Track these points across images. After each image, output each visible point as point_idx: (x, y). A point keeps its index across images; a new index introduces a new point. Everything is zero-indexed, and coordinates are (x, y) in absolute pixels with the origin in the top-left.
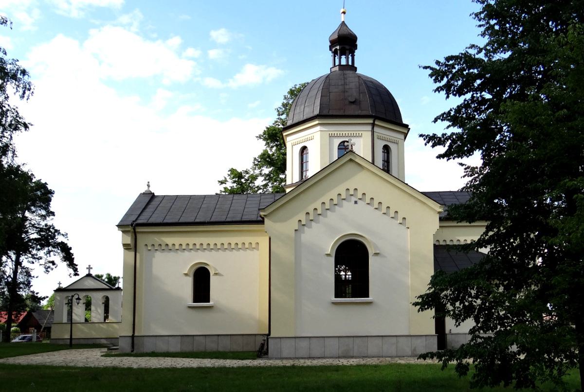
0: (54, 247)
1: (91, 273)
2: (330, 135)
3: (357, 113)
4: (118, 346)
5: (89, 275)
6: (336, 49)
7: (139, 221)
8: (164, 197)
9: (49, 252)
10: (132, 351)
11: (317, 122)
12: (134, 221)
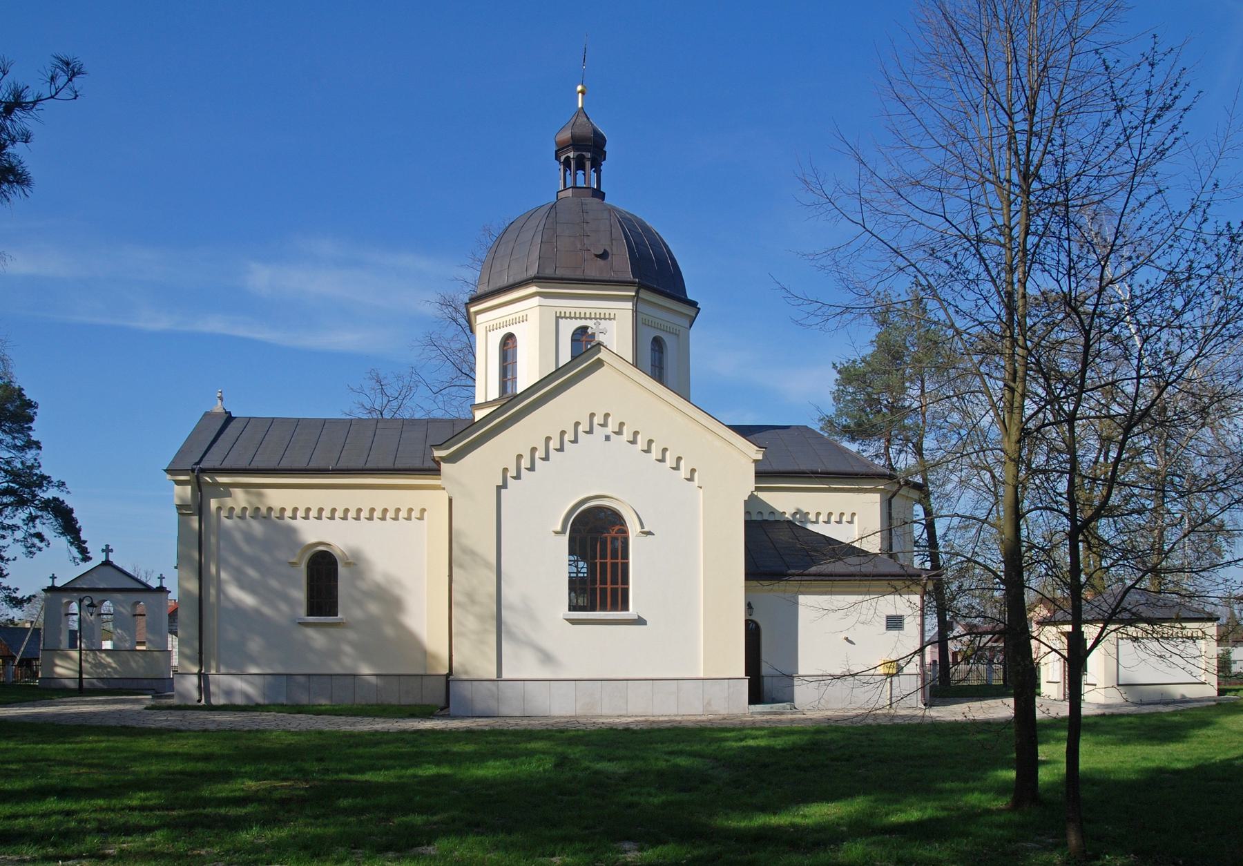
0: (41, 509)
2: (558, 315)
3: (605, 277)
4: (170, 696)
5: (107, 563)
6: (568, 159)
9: (32, 519)
11: (533, 289)
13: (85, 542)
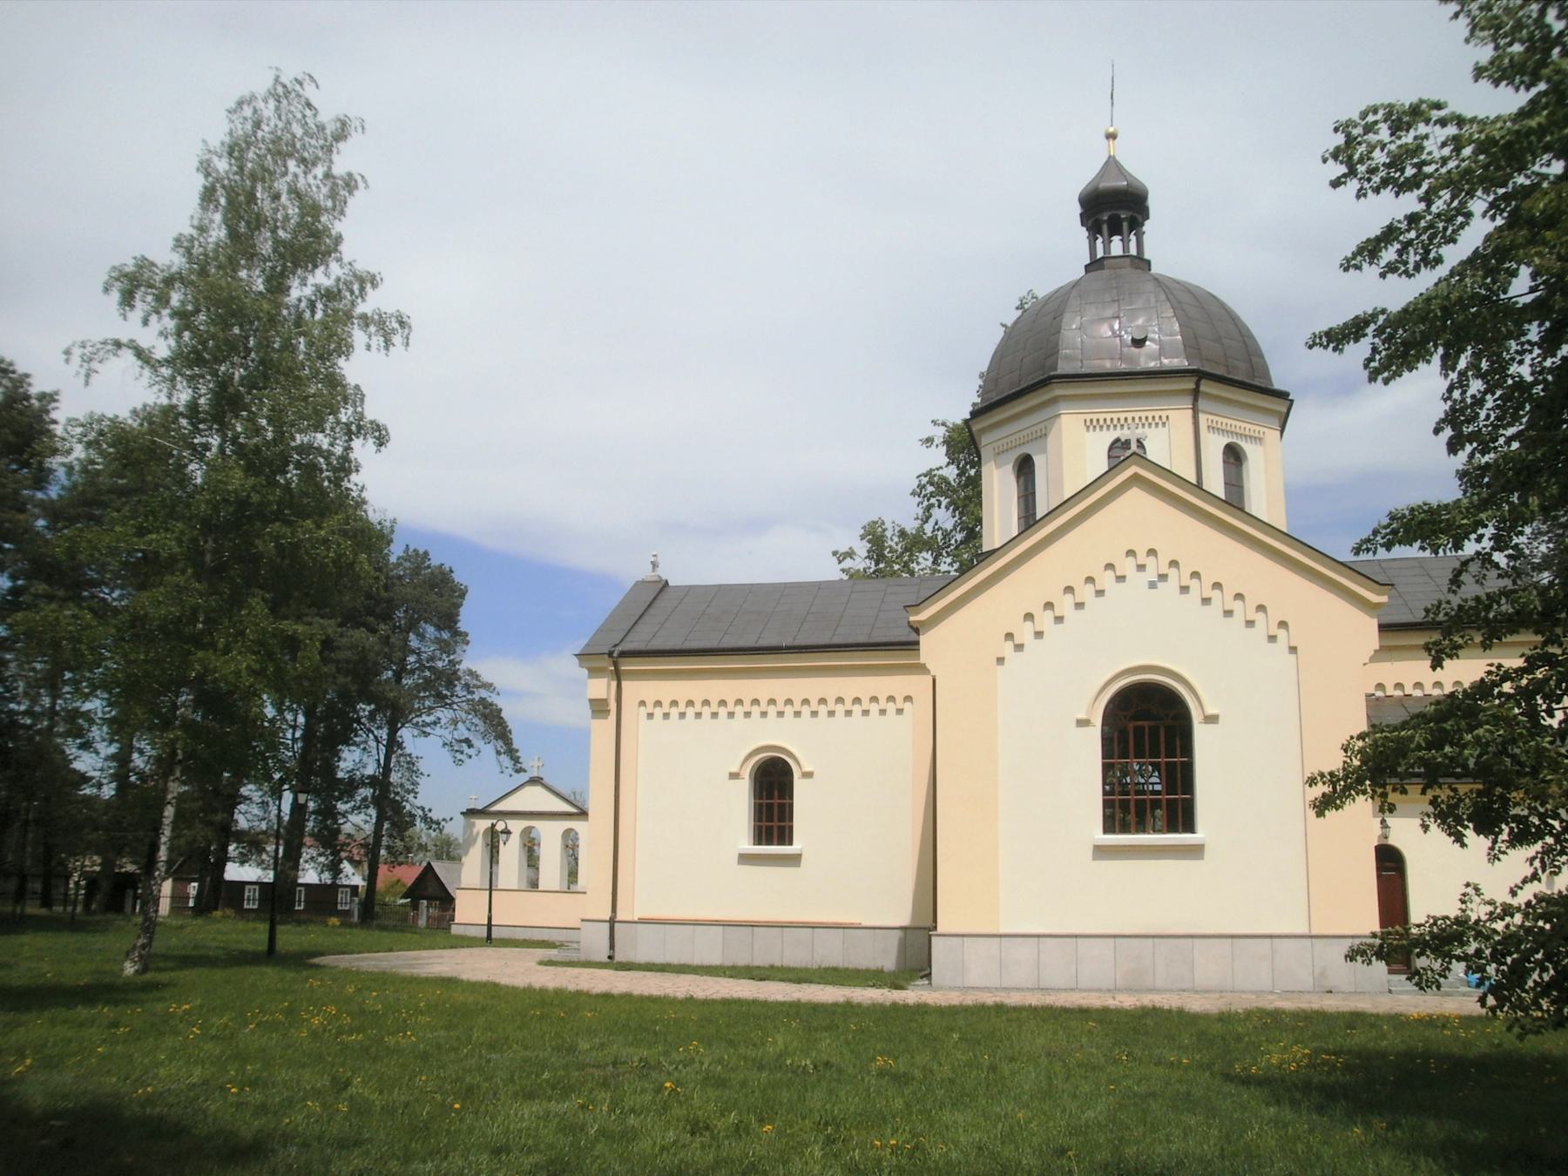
1: (1392, 841)
7: (626, 646)
8: (689, 590)
12: (616, 646)
13: (517, 751)
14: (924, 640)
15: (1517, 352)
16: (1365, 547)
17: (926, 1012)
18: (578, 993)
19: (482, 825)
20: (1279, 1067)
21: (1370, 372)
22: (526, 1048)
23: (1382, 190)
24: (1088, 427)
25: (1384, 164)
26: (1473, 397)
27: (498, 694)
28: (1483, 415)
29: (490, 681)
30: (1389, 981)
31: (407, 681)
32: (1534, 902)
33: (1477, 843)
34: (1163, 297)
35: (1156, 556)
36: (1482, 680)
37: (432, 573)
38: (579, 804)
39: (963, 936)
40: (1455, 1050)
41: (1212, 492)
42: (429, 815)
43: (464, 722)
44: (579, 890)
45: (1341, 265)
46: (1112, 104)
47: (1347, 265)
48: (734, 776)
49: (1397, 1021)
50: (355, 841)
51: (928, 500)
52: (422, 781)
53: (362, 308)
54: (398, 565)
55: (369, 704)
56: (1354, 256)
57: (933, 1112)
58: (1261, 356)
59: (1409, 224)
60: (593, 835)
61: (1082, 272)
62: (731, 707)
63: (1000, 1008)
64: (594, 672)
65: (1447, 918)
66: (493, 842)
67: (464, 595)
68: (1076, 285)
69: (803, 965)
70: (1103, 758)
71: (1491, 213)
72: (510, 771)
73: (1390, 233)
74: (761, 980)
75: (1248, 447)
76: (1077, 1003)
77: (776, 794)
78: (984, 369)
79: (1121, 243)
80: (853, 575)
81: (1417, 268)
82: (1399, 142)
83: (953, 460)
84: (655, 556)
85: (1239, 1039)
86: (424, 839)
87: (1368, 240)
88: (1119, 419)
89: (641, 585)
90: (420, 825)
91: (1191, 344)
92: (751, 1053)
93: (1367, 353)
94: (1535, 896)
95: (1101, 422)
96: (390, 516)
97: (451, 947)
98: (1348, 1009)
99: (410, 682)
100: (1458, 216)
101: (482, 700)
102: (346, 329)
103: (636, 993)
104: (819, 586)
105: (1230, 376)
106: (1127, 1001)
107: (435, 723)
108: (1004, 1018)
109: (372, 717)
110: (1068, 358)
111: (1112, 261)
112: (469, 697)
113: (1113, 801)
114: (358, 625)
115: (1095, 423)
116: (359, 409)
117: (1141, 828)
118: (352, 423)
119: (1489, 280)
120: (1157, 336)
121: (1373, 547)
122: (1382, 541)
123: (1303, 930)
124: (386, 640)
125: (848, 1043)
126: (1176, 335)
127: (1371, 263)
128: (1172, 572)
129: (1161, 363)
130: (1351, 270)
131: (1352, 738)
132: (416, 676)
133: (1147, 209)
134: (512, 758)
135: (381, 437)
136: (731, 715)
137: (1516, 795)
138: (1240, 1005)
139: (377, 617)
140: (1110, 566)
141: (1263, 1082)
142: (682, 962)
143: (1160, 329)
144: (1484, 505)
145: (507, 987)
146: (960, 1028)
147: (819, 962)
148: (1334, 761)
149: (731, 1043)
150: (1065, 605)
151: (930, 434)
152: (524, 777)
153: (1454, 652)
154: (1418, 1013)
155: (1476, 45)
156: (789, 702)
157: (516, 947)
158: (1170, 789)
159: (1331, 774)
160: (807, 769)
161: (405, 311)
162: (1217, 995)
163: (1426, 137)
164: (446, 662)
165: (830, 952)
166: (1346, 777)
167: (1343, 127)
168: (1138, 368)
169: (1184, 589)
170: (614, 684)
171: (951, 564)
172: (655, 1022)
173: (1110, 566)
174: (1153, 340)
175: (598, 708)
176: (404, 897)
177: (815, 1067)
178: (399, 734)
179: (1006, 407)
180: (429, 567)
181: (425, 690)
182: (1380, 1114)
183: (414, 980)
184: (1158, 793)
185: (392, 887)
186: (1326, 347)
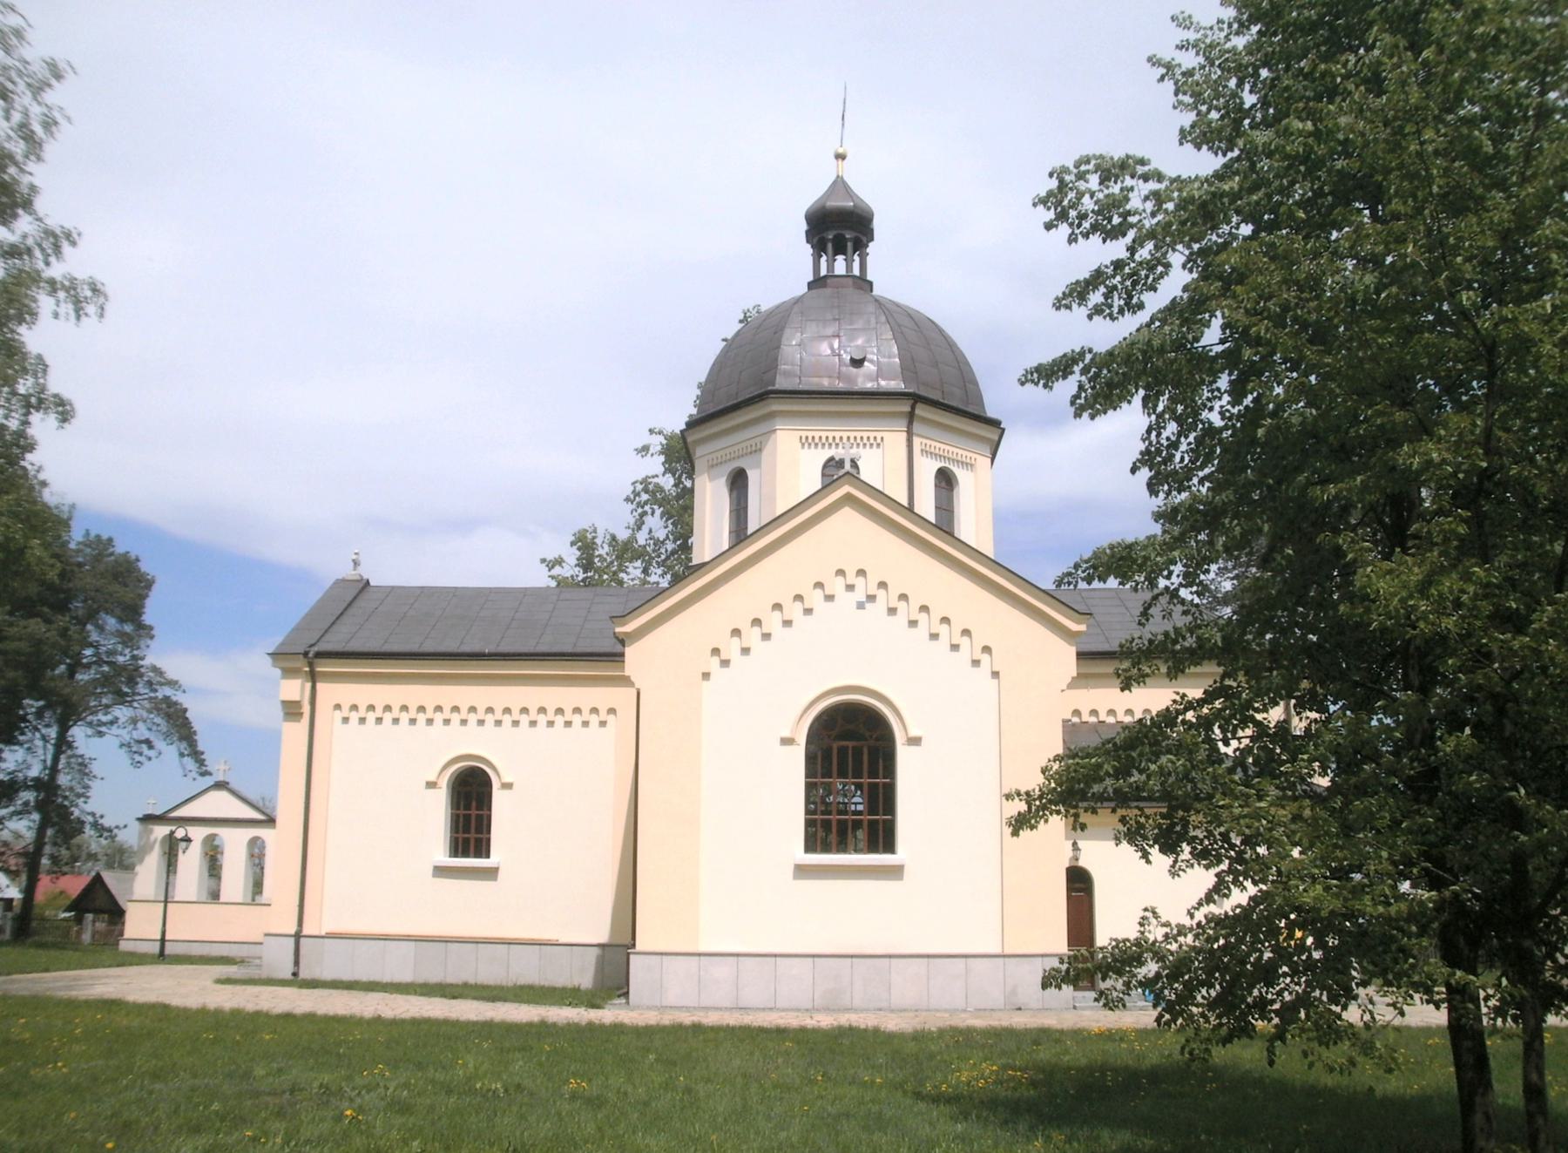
1: (1082, 863)
7: (330, 644)
10: (295, 974)
13: (202, 753)
14: (630, 652)
15: (1209, 399)
16: (1066, 580)
17: (623, 1032)
18: (258, 1014)
19: (161, 831)
20: (968, 1084)
21: (1076, 409)
22: (195, 1076)
23: (1091, 236)
24: (803, 445)
25: (1093, 211)
26: (1168, 439)
27: (184, 692)
28: (1177, 459)
29: (175, 678)
30: (1074, 998)
31: (82, 677)
32: (1204, 922)
33: (1161, 860)
34: (883, 319)
35: (865, 577)
36: (1168, 709)
37: (116, 561)
38: (268, 811)
39: (662, 954)
40: (1130, 1062)
41: (923, 515)
42: (101, 821)
43: (145, 721)
44: (263, 902)
45: (1054, 304)
46: (843, 125)
47: (1060, 304)
48: (431, 785)
49: (1079, 1036)
50: (12, 849)
51: (643, 507)
52: (95, 785)
53: (56, 271)
54: (78, 551)
55: (38, 700)
56: (1065, 296)
57: (626, 1136)
58: (976, 384)
59: (1115, 269)
60: (280, 844)
61: (805, 289)
62: (430, 714)
63: (697, 1028)
64: (289, 673)
65: (1128, 940)
66: (172, 849)
67: (151, 586)
68: (798, 301)
69: (499, 983)
70: (807, 777)
71: (1189, 266)
72: (194, 774)
73: (1097, 278)
74: (454, 997)
75: (959, 473)
76: (774, 1023)
77: (474, 804)
78: (703, 379)
79: (844, 263)
80: (562, 583)
81: (1121, 311)
82: (1106, 192)
83: (669, 470)
84: (356, 554)
85: (932, 1057)
86: (94, 847)
87: (1078, 282)
88: (834, 438)
89: (341, 583)
90: (89, 831)
91: (909, 367)
92: (440, 1076)
93: (1074, 390)
94: (1206, 917)
95: (817, 440)
96: (68, 500)
97: (118, 966)
98: (1035, 1026)
99: (86, 677)
100: (1158, 266)
101: (166, 699)
102: (29, 292)
103: (320, 1012)
104: (525, 592)
105: (946, 402)
106: (825, 1021)
107: (112, 723)
108: (701, 1038)
109: (39, 714)
110: (787, 374)
111: (836, 279)
112: (152, 695)
113: (815, 820)
114: (32, 615)
115: (810, 440)
116: (42, 381)
117: (842, 847)
118: (31, 395)
119: (1184, 329)
120: (875, 358)
121: (1074, 581)
122: (1083, 575)
123: (998, 950)
124: (64, 633)
125: (540, 1064)
126: (894, 357)
127: (1080, 305)
128: (881, 594)
129: (878, 384)
130: (1063, 309)
131: (1049, 761)
132: (93, 671)
133: (872, 231)
134: (196, 761)
135: (64, 411)
136: (430, 722)
137: (1194, 818)
138: (933, 1023)
139: (52, 607)
140: (819, 585)
141: (950, 1100)
142: (372, 979)
143: (878, 350)
144: (1179, 541)
145: (177, 1008)
146: (657, 1049)
147: (514, 980)
148: (1033, 781)
149: (420, 1066)
150: (773, 622)
151: (645, 442)
152: (209, 781)
153: (1141, 679)
154: (1099, 1027)
155: (1181, 111)
156: (490, 710)
157: (192, 963)
158: (872, 809)
159: (1028, 794)
160: (506, 779)
161: (100, 277)
162: (912, 1014)
163: (1132, 189)
164: (128, 657)
165: (526, 970)
166: (1041, 797)
167: (1059, 173)
168: (856, 388)
169: (892, 611)
170: (309, 685)
171: (662, 576)
172: (339, 1044)
173: (819, 585)
174: (871, 361)
175: (291, 710)
176: (68, 909)
177: (506, 1091)
178: (70, 733)
179: (722, 419)
180: (112, 554)
181: (103, 686)
182: (1059, 1127)
183: (72, 1005)
184: (860, 813)
185: (55, 898)
186: (1037, 384)
